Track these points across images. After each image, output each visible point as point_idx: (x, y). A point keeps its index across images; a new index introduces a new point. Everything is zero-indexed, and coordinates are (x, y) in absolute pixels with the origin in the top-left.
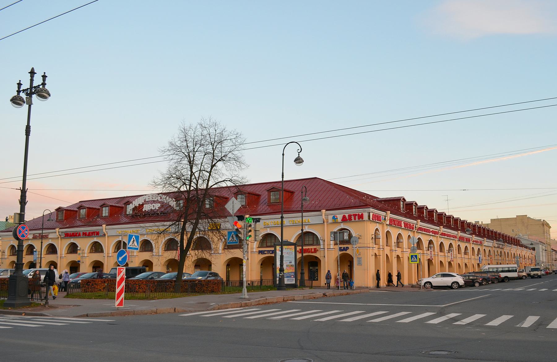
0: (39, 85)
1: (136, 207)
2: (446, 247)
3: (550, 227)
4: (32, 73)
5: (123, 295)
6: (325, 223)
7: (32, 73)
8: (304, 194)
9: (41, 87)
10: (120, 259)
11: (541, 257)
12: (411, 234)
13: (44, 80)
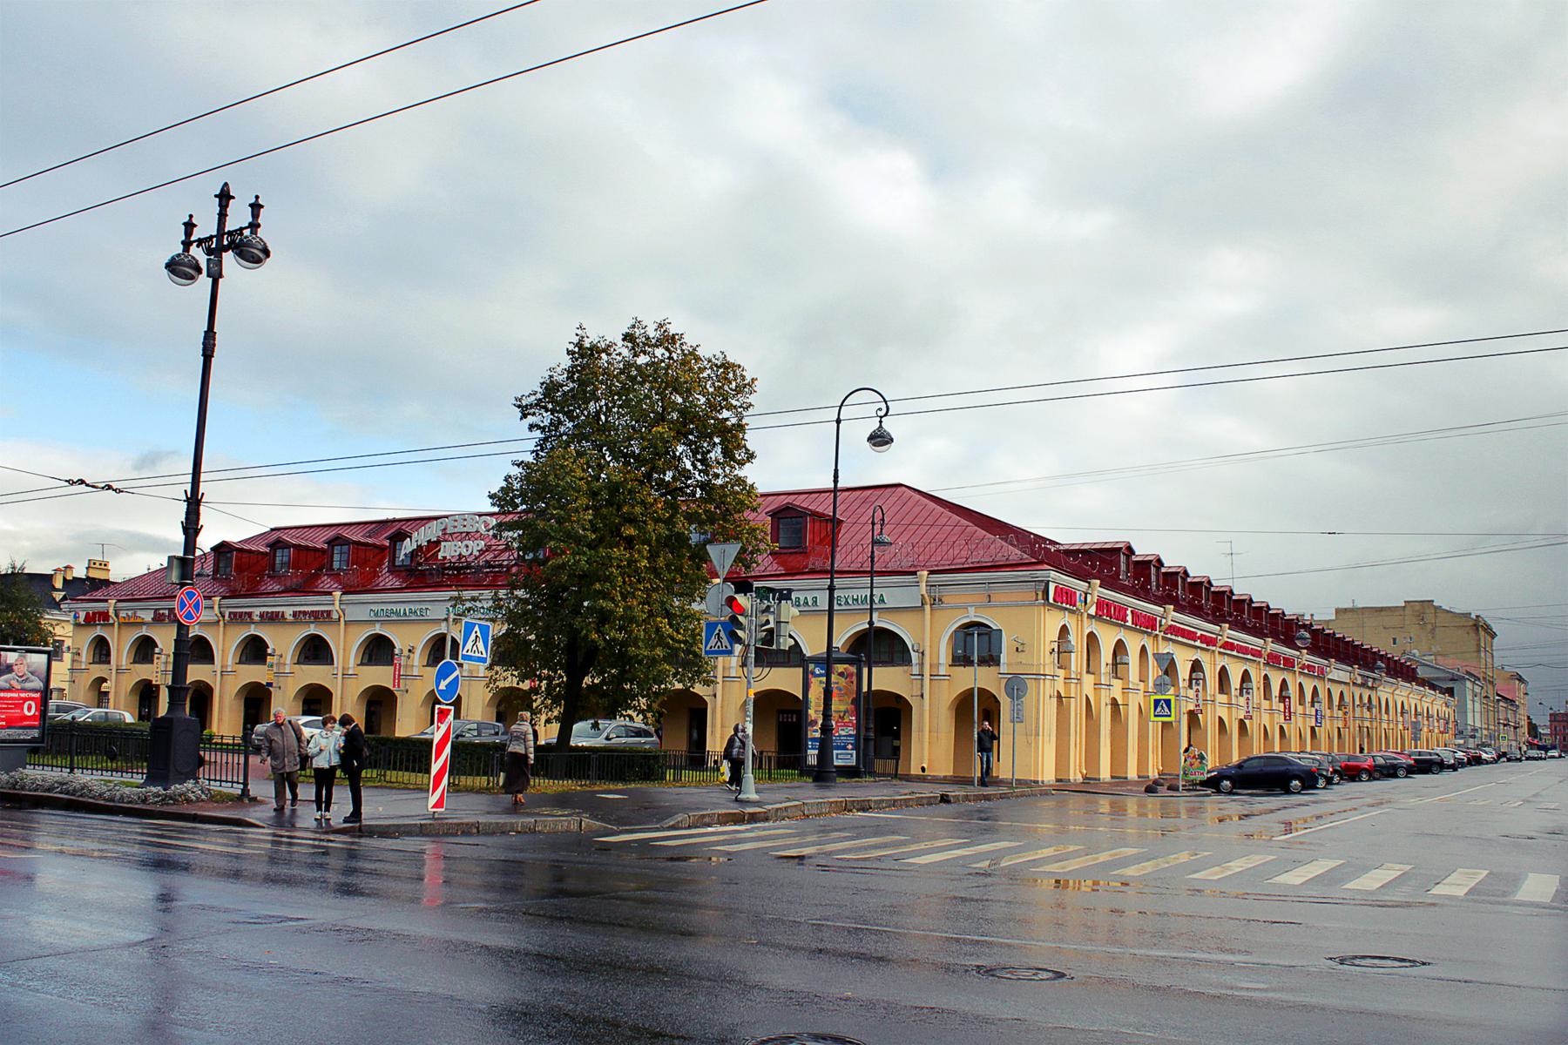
0: (241, 229)
1: (420, 547)
2: (1235, 681)
3: (1493, 635)
4: (224, 197)
5: (445, 781)
6: (927, 607)
7: (224, 197)
8: (877, 527)
9: (247, 232)
10: (443, 685)
11: (1470, 715)
12: (1148, 642)
13: (255, 215)
